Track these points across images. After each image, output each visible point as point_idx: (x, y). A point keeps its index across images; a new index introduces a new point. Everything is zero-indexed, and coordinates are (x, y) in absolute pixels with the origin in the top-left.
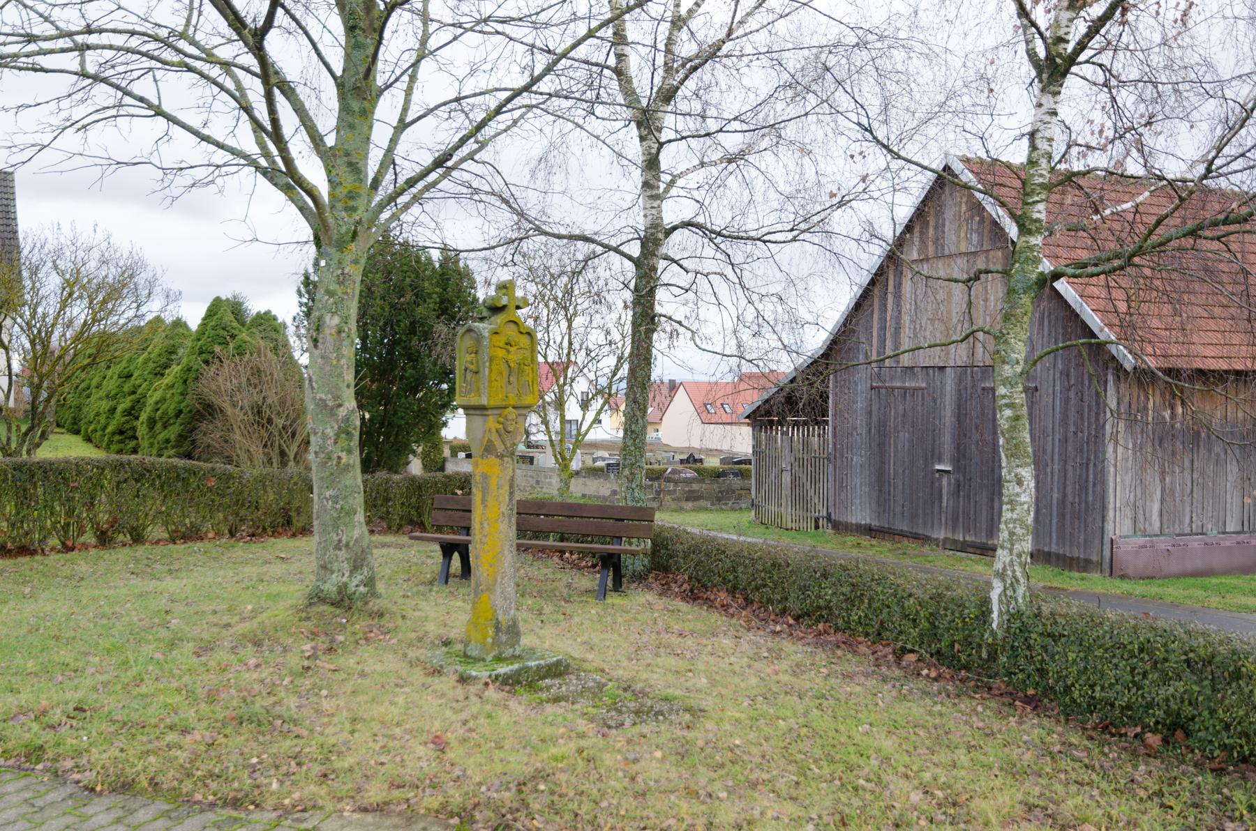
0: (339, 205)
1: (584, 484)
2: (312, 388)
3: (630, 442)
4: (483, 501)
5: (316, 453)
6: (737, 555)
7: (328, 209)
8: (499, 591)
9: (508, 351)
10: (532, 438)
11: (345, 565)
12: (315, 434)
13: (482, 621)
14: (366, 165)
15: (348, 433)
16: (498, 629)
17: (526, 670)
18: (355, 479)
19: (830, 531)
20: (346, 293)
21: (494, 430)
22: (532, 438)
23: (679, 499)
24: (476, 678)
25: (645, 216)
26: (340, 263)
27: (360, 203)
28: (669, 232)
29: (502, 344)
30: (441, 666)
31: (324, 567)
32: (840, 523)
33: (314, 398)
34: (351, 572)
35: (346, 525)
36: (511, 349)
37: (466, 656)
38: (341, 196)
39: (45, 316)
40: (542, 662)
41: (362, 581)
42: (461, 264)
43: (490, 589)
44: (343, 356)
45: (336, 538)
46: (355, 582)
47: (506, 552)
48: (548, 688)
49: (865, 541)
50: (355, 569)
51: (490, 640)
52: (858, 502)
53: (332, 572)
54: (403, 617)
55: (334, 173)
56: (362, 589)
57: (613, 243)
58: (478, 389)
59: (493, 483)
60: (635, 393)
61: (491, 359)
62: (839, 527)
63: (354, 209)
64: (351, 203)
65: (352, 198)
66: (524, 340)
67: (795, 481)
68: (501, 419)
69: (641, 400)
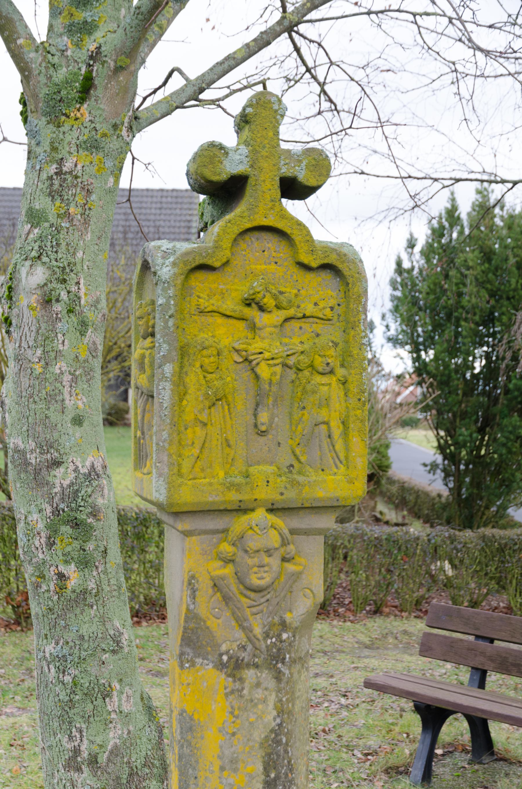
9: (253, 327)
20: (67, 215)
26: (54, 149)
35: (87, 720)
44: (59, 354)
68: (226, 548)
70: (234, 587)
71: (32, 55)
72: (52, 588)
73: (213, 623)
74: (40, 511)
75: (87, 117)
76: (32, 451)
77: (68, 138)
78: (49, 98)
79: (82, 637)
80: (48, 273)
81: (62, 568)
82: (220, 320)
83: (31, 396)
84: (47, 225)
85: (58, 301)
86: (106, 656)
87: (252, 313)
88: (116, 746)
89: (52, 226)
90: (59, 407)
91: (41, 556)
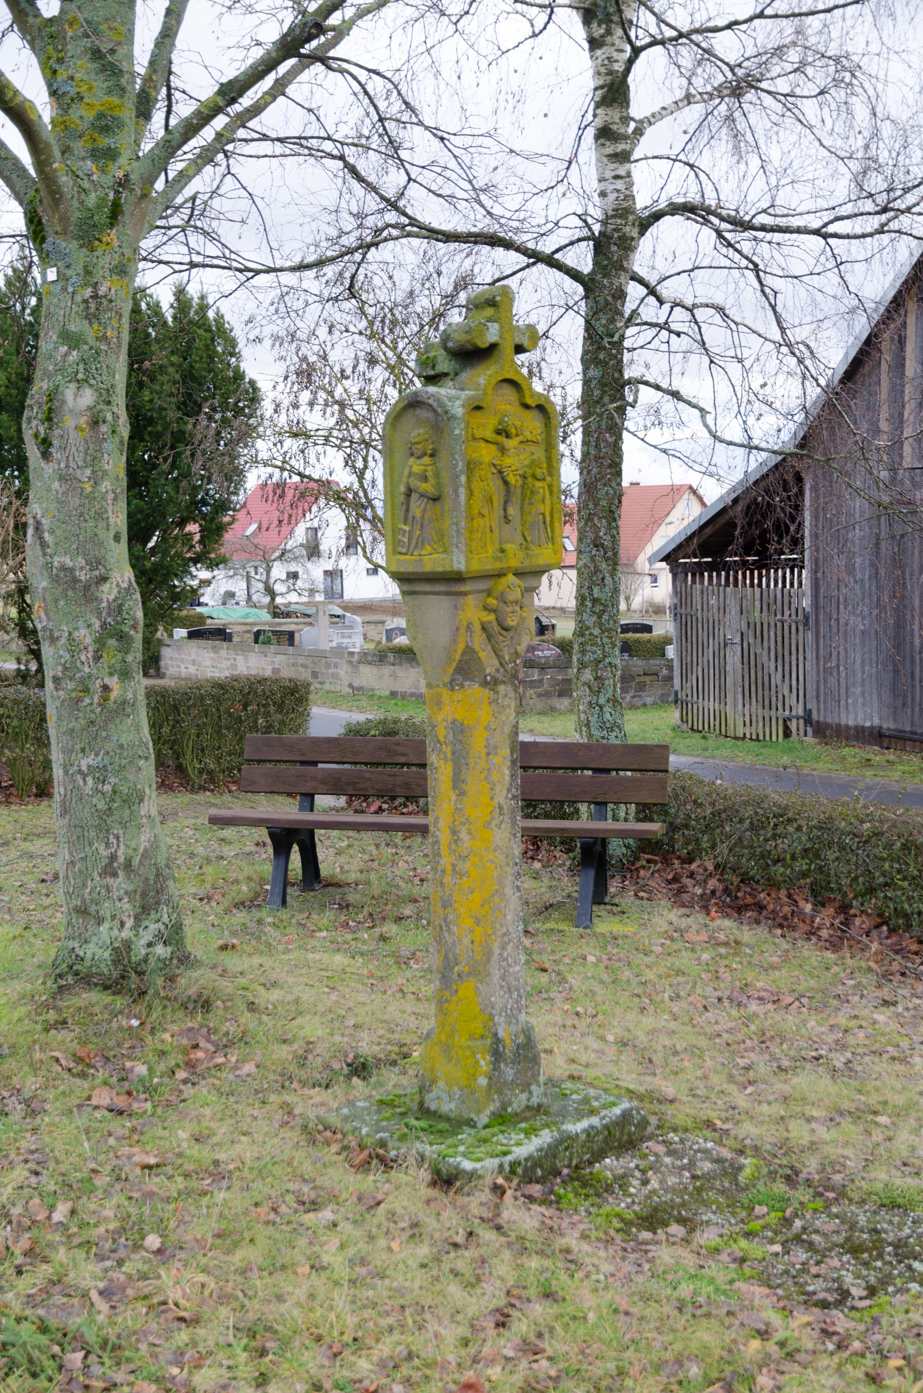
0: (79, 147)
1: (394, 675)
2: (43, 545)
3: (590, 621)
4: (457, 782)
5: (56, 679)
6: (825, 826)
7: (57, 153)
8: (496, 974)
9: (503, 450)
10: (279, 600)
11: (126, 905)
12: (53, 640)
13: (461, 1040)
14: (130, 57)
15: (122, 637)
16: (497, 1055)
17: (567, 1141)
18: (138, 729)
19: (810, 739)
20: (105, 338)
21: (477, 627)
22: (279, 600)
23: (547, 694)
24: (472, 1175)
25: (603, 194)
26: (88, 272)
27: (121, 140)
28: (645, 224)
29: (489, 434)
30: (383, 1144)
31: (82, 912)
32: (828, 726)
33: (49, 566)
34: (137, 918)
35: (124, 825)
36: (511, 443)
37: (424, 1111)
38: (83, 126)
39: (828, 1290)
40: (595, 1121)
41: (159, 935)
42: (211, 314)
43: (478, 972)
45: (104, 853)
46: (147, 936)
47: (509, 891)
48: (622, 1180)
49: (878, 756)
50: (145, 910)
51: (483, 1081)
52: (859, 690)
53: (100, 921)
54: (252, 1007)
55: (62, 75)
56: (160, 950)
57: (547, 246)
58: (441, 535)
59: (478, 741)
60: (596, 529)
61: (471, 467)
62: (822, 731)
63: (111, 154)
64: (105, 141)
65: (106, 130)
66: (532, 425)
67: (747, 659)
68: (492, 601)
69: (607, 541)
70: (497, 628)
71: (64, 179)
72: (96, 700)
73: (482, 655)
74: (89, 626)
75: (116, 243)
76: (82, 568)
77: (101, 263)
78: (81, 223)
79: (121, 747)
80: (96, 395)
81: (107, 681)
82: (483, 444)
83: (81, 515)
84: (86, 347)
85: (104, 422)
86: (141, 763)
87: (501, 439)
88: (146, 850)
89: (91, 348)
90: (104, 524)
91: (87, 670)
